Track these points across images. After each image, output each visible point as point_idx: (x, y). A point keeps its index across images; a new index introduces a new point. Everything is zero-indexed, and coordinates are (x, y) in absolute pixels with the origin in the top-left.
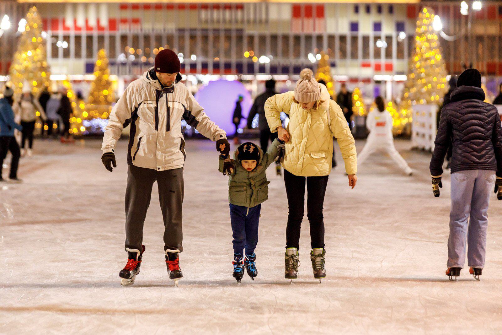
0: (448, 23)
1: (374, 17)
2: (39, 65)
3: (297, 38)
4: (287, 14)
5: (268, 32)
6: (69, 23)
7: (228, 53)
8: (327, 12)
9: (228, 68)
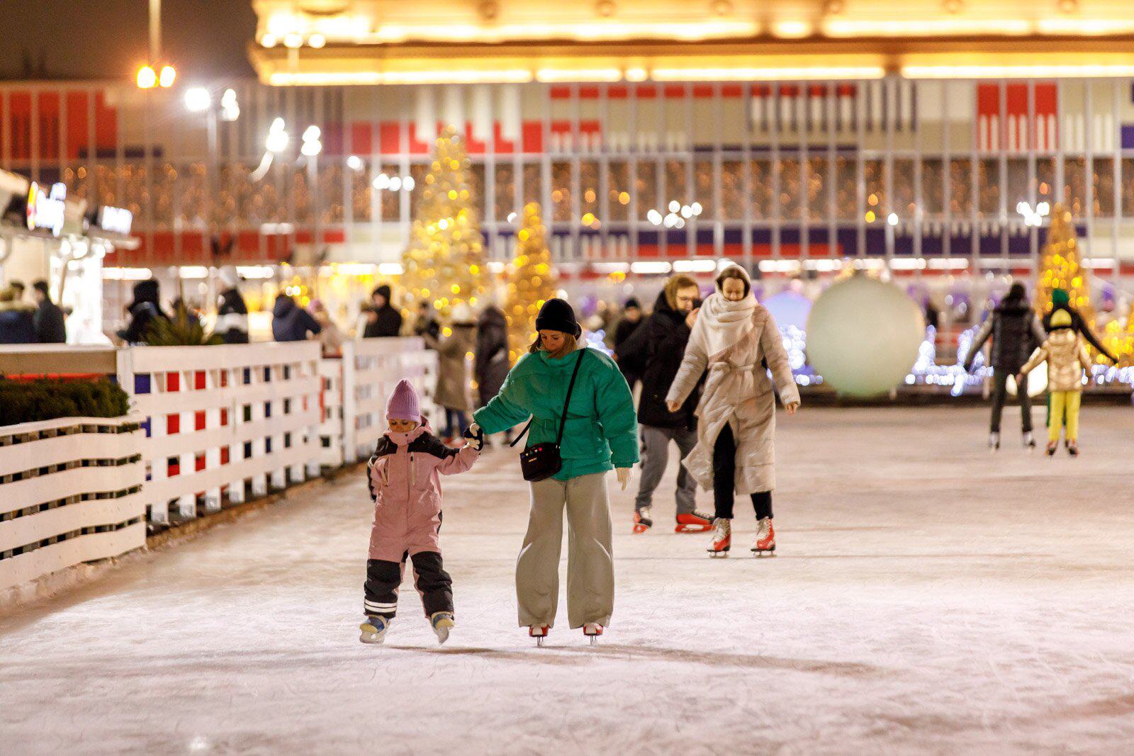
2: (464, 248)
3: (990, 165)
4: (963, 108)
5: (915, 151)
6: (426, 133)
7: (818, 204)
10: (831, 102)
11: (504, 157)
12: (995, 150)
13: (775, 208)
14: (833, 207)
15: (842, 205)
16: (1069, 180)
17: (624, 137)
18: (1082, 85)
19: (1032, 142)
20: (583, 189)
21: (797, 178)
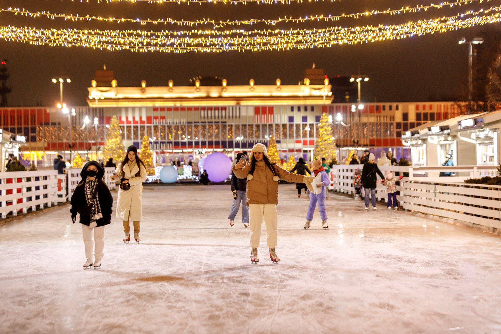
0: (346, 116)
1: (303, 113)
3: (258, 126)
4: (251, 113)
7: (217, 136)
8: (275, 111)
9: (217, 144)
10: (220, 111)
11: (143, 125)
12: (259, 123)
13: (207, 137)
14: (220, 136)
15: (223, 136)
16: (276, 130)
17: (171, 120)
18: (280, 107)
19: (267, 121)
20: (161, 132)
21: (212, 130)
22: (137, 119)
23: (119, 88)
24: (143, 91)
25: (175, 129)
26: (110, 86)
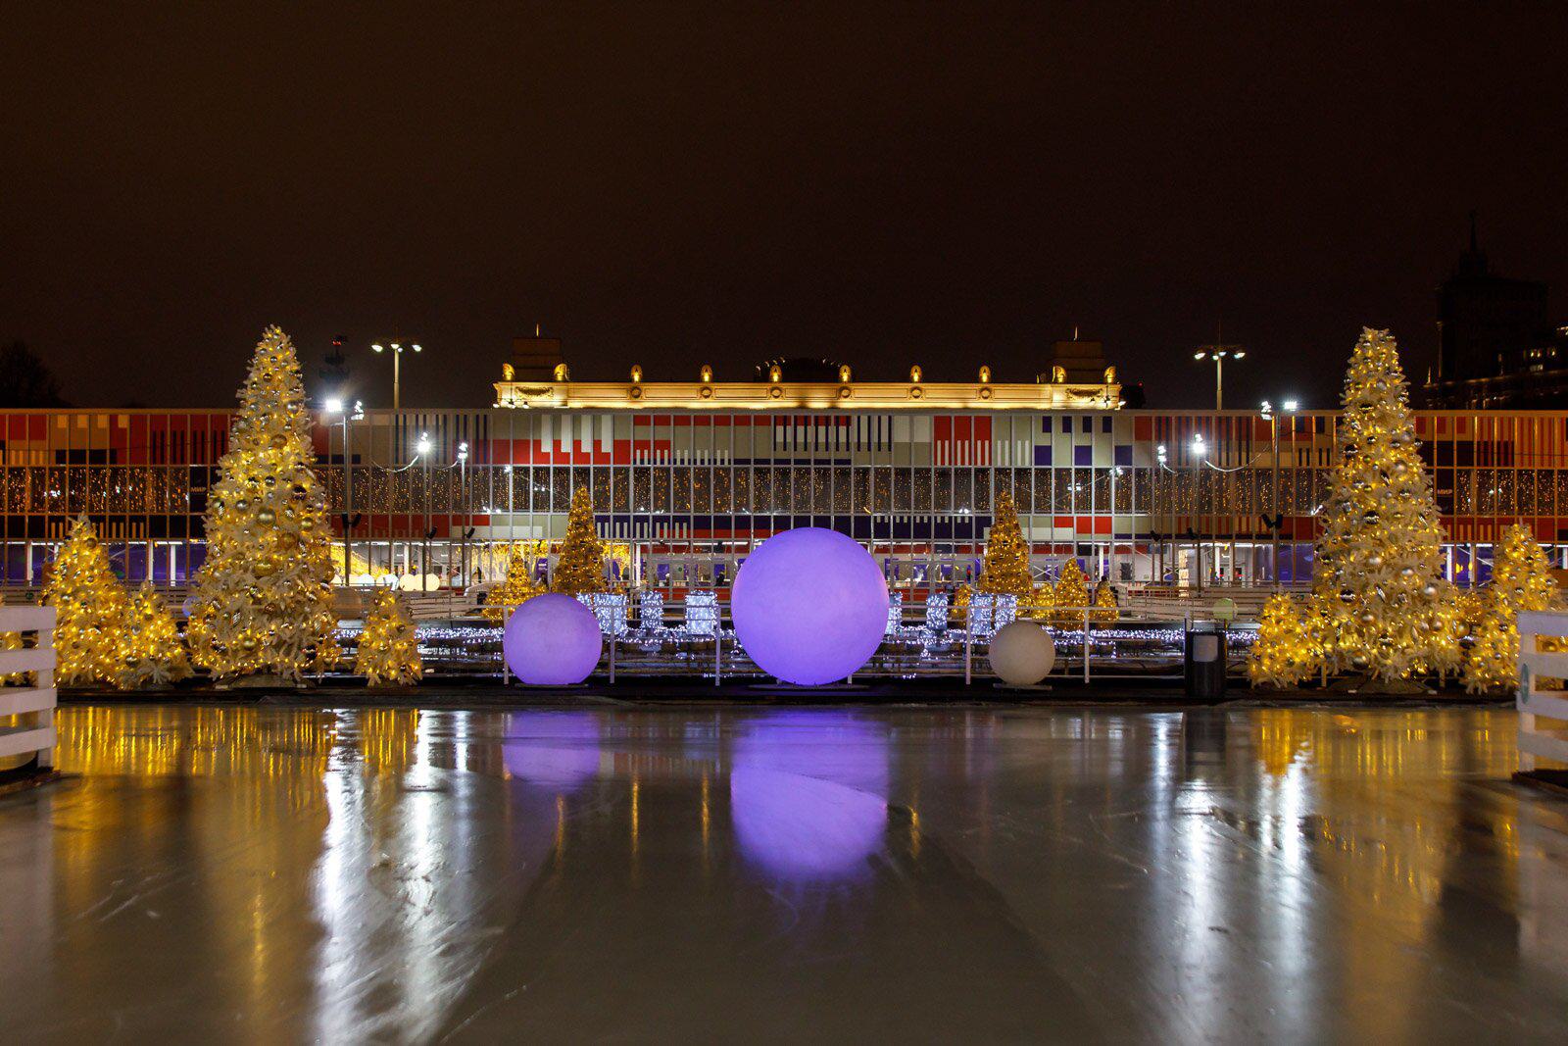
1: (1078, 439)
3: (943, 474)
4: (924, 433)
6: (547, 447)
7: (822, 500)
22: (587, 447)
23: (571, 385)
24: (635, 394)
25: (697, 479)
26: (552, 379)
